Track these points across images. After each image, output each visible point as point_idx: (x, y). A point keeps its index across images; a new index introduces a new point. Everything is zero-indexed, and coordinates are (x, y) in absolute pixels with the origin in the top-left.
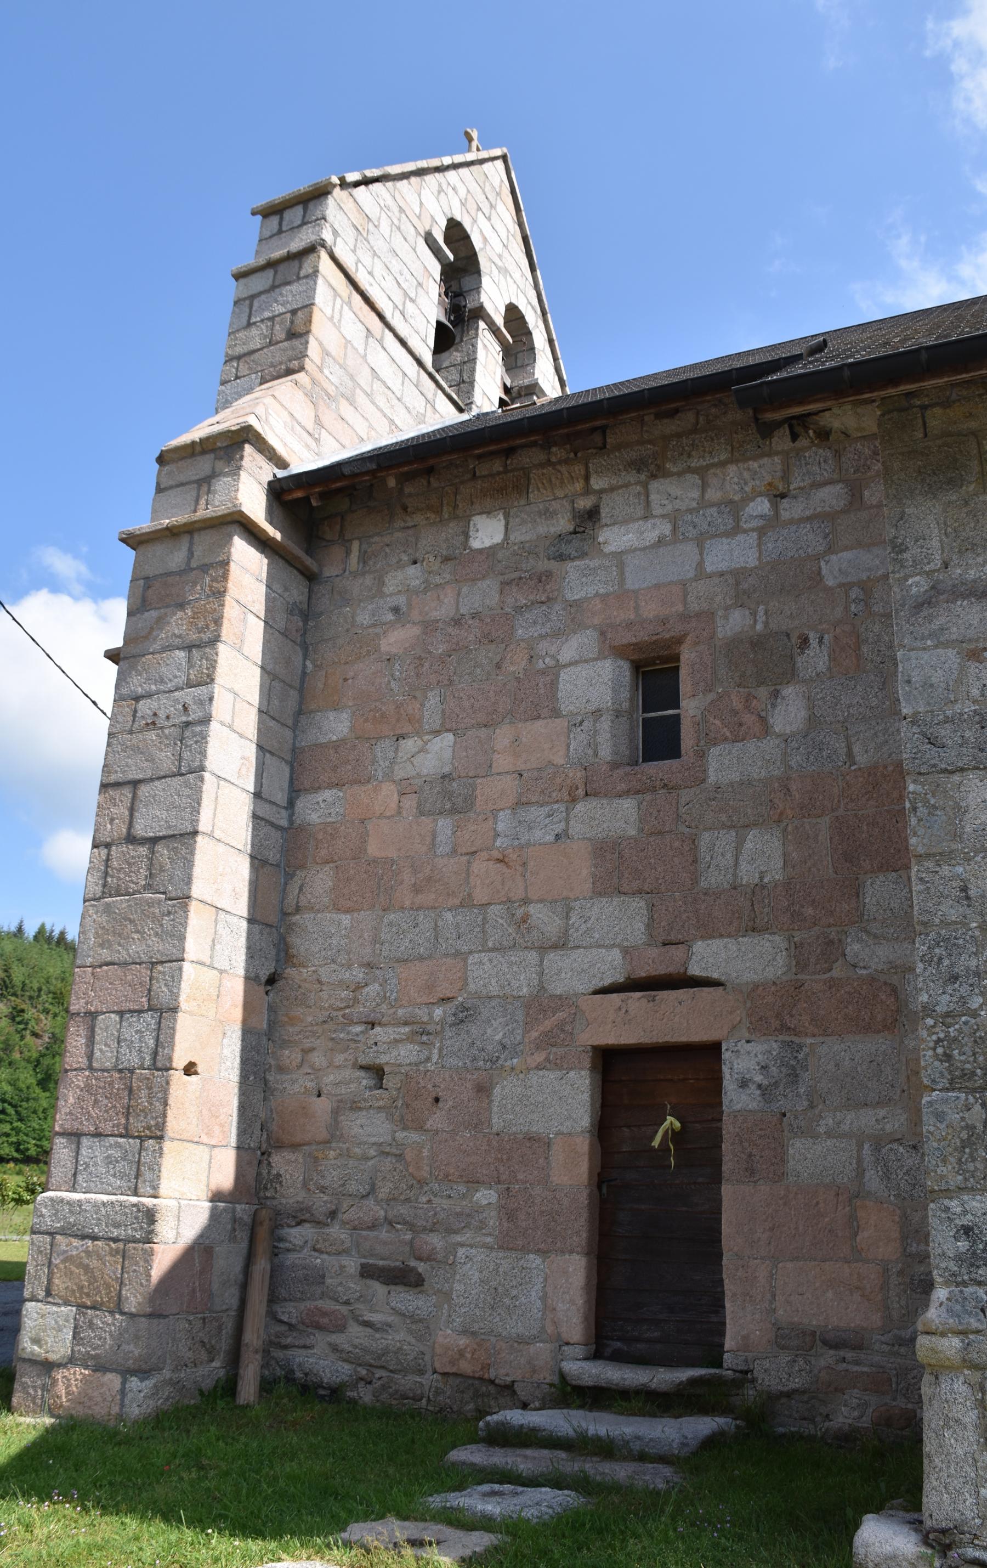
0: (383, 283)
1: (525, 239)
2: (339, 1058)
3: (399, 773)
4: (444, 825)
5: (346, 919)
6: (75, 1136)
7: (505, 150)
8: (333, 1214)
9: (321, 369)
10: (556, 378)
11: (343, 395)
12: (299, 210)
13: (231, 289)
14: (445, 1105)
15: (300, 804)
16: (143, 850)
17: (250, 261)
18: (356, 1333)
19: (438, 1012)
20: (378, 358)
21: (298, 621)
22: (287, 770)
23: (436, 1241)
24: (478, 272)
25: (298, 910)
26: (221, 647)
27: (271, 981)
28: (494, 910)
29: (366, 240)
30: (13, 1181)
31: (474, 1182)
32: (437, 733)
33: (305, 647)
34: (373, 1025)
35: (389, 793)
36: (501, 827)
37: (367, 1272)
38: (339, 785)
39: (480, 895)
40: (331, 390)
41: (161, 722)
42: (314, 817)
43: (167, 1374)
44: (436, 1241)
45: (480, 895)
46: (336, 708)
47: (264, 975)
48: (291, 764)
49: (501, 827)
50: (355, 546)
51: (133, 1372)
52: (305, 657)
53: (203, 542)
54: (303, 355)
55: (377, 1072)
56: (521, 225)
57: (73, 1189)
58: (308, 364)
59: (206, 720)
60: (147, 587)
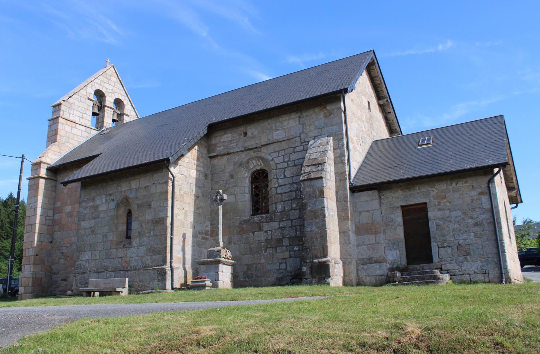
0: (77, 114)
1: (120, 81)
2: (59, 252)
3: (65, 212)
4: (70, 219)
5: (60, 233)
6: (24, 265)
7: (112, 65)
8: (58, 273)
9: (60, 140)
10: (132, 108)
11: (66, 142)
12: (57, 107)
13: (47, 123)
14: (69, 257)
15: (55, 216)
16: (30, 226)
17: (51, 118)
18: (61, 287)
19: (69, 245)
20: (75, 131)
21: (54, 188)
22: (53, 211)
23: (68, 275)
24: (105, 97)
25: (55, 231)
26: (39, 197)
27: (51, 242)
28: (74, 231)
29: (72, 108)
30: (534, 318)
31: (72, 267)
32: (69, 205)
33: (55, 192)
34: (62, 247)
35: (64, 214)
36: (75, 219)
37: (62, 280)
38: (59, 213)
39: (73, 229)
40: (63, 142)
41: (32, 207)
42: (56, 218)
43: (35, 293)
44: (68, 275)
45: (73, 229)
46: (59, 201)
47: (50, 241)
48: (54, 210)
49: (75, 219)
50: (61, 175)
51: (30, 293)
52: (55, 193)
53: (37, 179)
54: (56, 139)
55: (62, 253)
56: (119, 79)
57: (98, 279)
58: (57, 140)
59: (37, 207)
60: (30, 187)
